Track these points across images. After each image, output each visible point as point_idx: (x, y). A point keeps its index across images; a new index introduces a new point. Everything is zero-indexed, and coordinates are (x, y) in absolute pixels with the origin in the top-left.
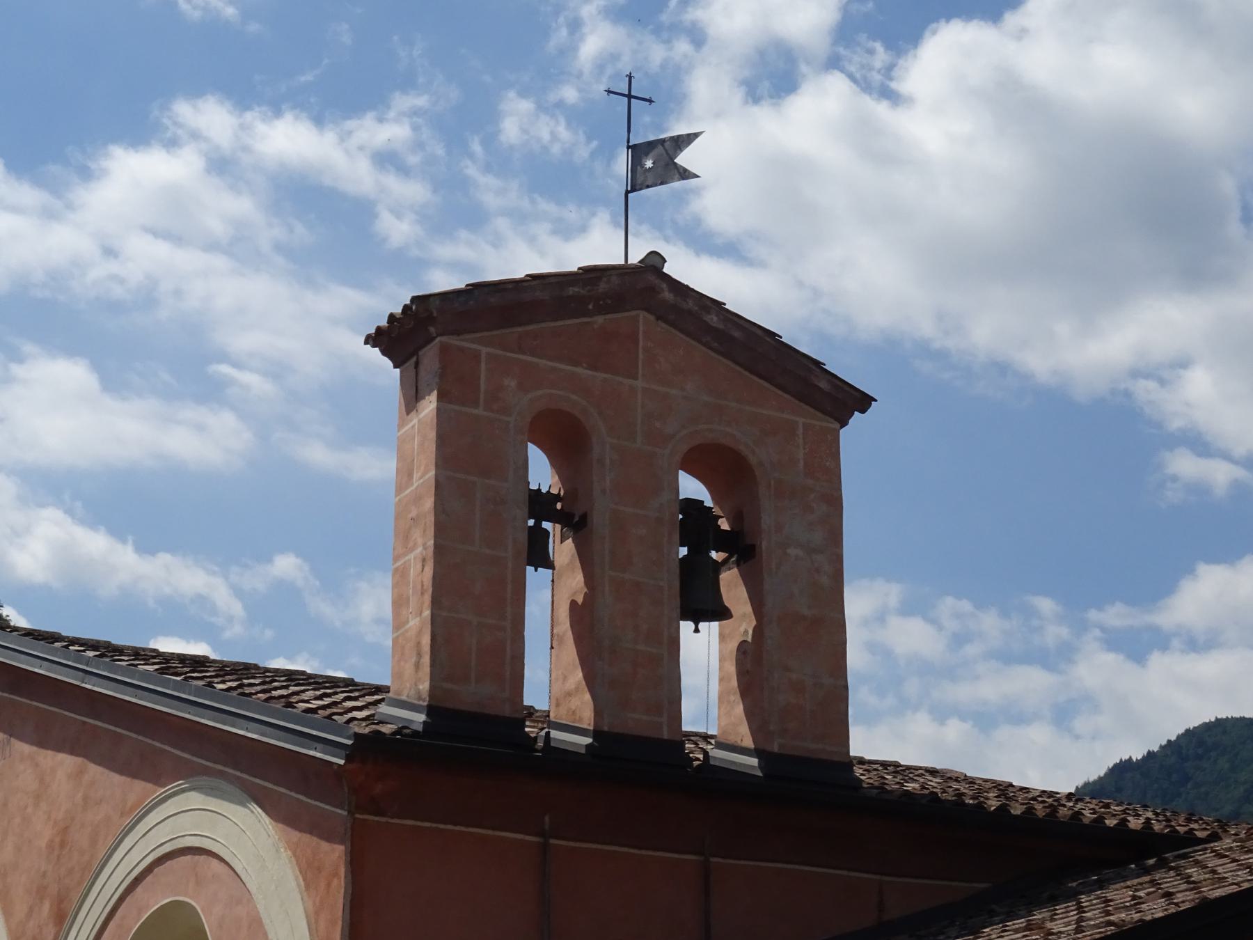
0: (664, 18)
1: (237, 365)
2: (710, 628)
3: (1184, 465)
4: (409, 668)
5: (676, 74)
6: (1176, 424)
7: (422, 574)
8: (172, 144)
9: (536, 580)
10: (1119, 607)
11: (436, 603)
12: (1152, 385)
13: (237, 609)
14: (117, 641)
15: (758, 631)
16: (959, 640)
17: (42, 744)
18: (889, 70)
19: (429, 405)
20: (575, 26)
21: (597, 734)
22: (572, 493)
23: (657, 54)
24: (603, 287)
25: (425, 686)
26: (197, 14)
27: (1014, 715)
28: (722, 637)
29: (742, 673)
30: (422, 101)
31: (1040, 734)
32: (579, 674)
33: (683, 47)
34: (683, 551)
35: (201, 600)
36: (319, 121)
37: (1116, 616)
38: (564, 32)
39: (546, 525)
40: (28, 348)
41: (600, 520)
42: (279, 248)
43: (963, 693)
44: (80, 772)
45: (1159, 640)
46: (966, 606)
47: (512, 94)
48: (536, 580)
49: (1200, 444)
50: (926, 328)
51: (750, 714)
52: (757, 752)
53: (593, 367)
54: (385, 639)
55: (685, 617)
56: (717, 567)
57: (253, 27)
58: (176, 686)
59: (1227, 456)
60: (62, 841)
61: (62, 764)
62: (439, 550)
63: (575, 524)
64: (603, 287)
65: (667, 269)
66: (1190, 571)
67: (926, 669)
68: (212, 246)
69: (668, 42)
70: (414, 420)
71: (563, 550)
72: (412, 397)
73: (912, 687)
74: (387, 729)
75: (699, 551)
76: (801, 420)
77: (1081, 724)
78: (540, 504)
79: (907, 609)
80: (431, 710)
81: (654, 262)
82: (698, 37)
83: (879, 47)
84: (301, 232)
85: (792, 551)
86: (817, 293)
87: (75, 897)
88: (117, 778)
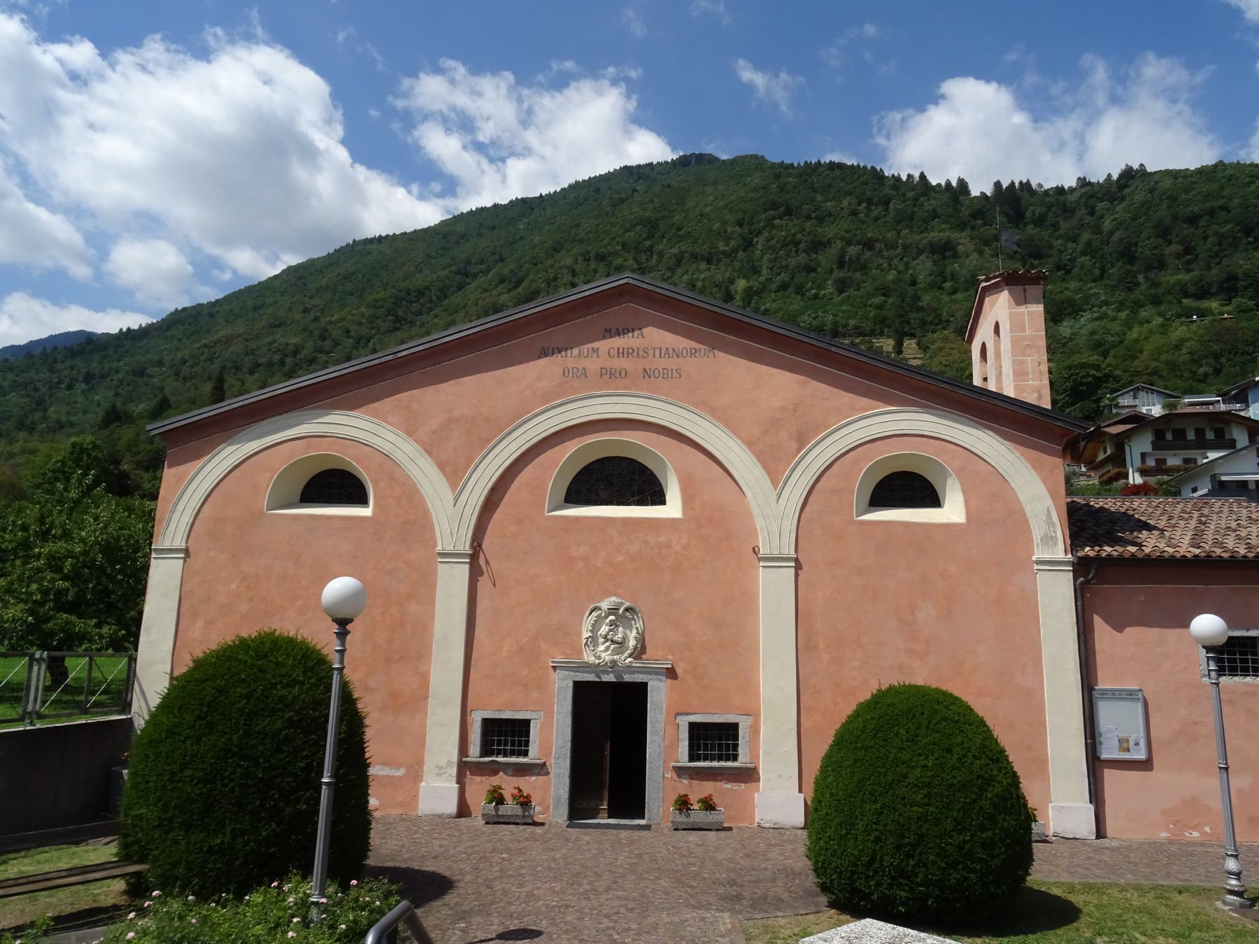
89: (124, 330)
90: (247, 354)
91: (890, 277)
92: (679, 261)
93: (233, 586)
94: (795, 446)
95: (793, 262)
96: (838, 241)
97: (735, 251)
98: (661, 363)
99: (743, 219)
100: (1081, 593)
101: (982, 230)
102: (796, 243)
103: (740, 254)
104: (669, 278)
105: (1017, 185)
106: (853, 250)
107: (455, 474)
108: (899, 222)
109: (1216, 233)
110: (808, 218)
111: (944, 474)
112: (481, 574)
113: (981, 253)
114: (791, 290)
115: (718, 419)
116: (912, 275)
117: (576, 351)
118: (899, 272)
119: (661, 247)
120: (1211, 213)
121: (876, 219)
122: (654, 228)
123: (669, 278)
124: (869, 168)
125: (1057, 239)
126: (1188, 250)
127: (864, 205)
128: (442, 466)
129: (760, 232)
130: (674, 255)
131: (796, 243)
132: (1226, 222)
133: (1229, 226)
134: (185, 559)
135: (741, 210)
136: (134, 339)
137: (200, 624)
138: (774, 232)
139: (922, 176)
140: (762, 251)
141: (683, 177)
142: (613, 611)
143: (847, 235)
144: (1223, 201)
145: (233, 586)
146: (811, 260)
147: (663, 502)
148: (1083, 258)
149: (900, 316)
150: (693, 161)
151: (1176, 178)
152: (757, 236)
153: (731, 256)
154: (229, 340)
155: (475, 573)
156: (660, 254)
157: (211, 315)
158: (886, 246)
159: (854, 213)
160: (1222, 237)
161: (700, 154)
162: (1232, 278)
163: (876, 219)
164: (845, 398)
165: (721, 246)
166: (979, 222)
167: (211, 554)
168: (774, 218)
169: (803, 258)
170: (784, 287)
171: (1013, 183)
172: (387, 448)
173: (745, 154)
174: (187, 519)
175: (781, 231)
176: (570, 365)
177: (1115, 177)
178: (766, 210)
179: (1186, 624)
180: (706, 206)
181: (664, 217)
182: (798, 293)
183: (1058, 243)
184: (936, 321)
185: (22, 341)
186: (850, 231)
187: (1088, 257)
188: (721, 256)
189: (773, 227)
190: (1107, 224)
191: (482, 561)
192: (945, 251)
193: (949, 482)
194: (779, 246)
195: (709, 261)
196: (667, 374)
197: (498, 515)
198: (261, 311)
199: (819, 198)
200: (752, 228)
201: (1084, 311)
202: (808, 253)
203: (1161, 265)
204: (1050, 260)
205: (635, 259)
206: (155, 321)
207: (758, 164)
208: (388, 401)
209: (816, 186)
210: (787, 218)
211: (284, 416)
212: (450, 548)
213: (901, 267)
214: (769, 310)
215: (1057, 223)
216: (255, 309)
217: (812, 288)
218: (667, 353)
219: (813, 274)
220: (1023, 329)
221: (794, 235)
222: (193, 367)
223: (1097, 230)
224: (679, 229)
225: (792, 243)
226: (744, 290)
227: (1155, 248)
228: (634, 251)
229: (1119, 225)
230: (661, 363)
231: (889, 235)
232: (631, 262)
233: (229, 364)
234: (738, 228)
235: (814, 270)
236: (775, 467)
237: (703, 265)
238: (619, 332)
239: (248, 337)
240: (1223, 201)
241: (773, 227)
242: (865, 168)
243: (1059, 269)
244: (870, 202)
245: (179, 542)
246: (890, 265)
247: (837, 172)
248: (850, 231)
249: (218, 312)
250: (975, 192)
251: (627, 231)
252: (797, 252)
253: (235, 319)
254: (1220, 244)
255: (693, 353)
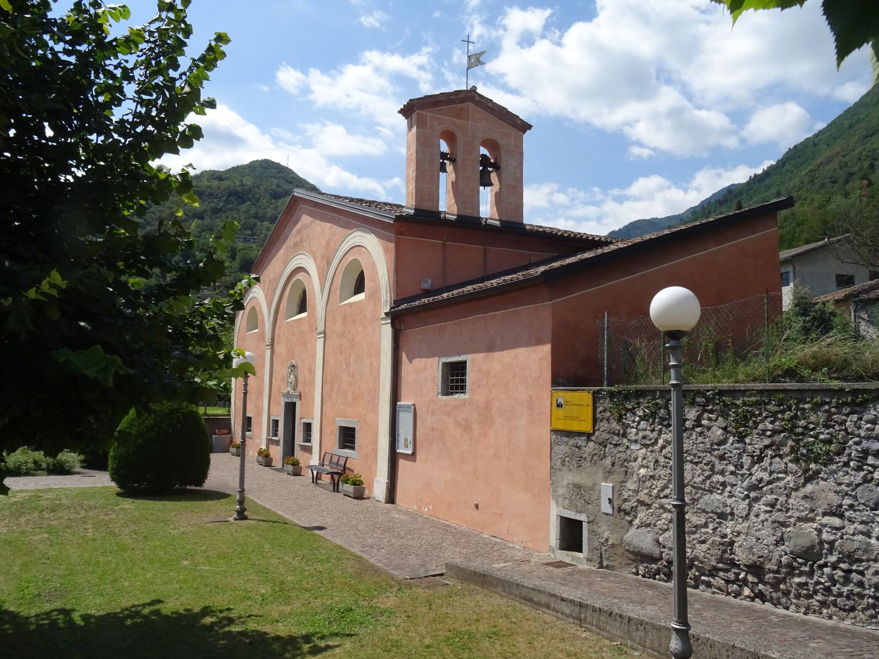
0: (497, 23)
1: (383, 127)
2: (488, 188)
3: (636, 150)
4: (410, 198)
5: (499, 39)
6: (634, 138)
7: (413, 175)
8: (365, 64)
9: (442, 175)
10: (617, 189)
11: (416, 182)
12: (628, 127)
13: (383, 192)
14: (341, 195)
15: (500, 189)
16: (573, 199)
17: (322, 220)
18: (561, 37)
19: (414, 129)
20: (472, 26)
21: (458, 215)
22: (452, 154)
23: (494, 33)
24: (460, 96)
25: (414, 203)
26: (368, 25)
27: (587, 219)
28: (491, 191)
29: (496, 200)
30: (430, 49)
31: (593, 224)
32: (454, 200)
33: (501, 32)
34: (481, 168)
35: (374, 190)
36: (403, 56)
37: (616, 192)
38: (469, 28)
39: (445, 161)
40: (328, 122)
41: (459, 160)
42: (393, 94)
43: (573, 213)
44: (332, 227)
45: (627, 198)
46: (575, 190)
47: (456, 48)
48: (442, 175)
49: (640, 144)
50: (568, 113)
51: (498, 210)
52: (500, 220)
53: (457, 119)
54: (404, 191)
55: (481, 185)
56: (490, 172)
57: (383, 29)
58: (353, 205)
59: (648, 148)
60: (328, 244)
61: (327, 225)
62: (417, 168)
63: (453, 161)
64: (460, 96)
65: (477, 91)
66: (637, 180)
67: (564, 207)
68: (375, 93)
69: (497, 30)
70: (411, 133)
71: (449, 167)
72: (410, 127)
73: (560, 212)
74: (404, 214)
75: (485, 168)
76: (513, 132)
77: (604, 221)
78: (444, 156)
79: (560, 191)
80: (415, 209)
81: (474, 89)
82: (505, 29)
83: (557, 31)
84: (398, 89)
85: (509, 168)
86: (537, 103)
87: (331, 258)
88: (340, 229)
89: (752, 176)
90: (841, 168)
136: (759, 181)
154: (829, 160)
157: (815, 145)
185: (696, 203)
198: (856, 128)
206: (774, 163)
216: (850, 127)
222: (799, 191)
233: (827, 181)
239: (846, 153)
249: (820, 140)
253: (835, 141)
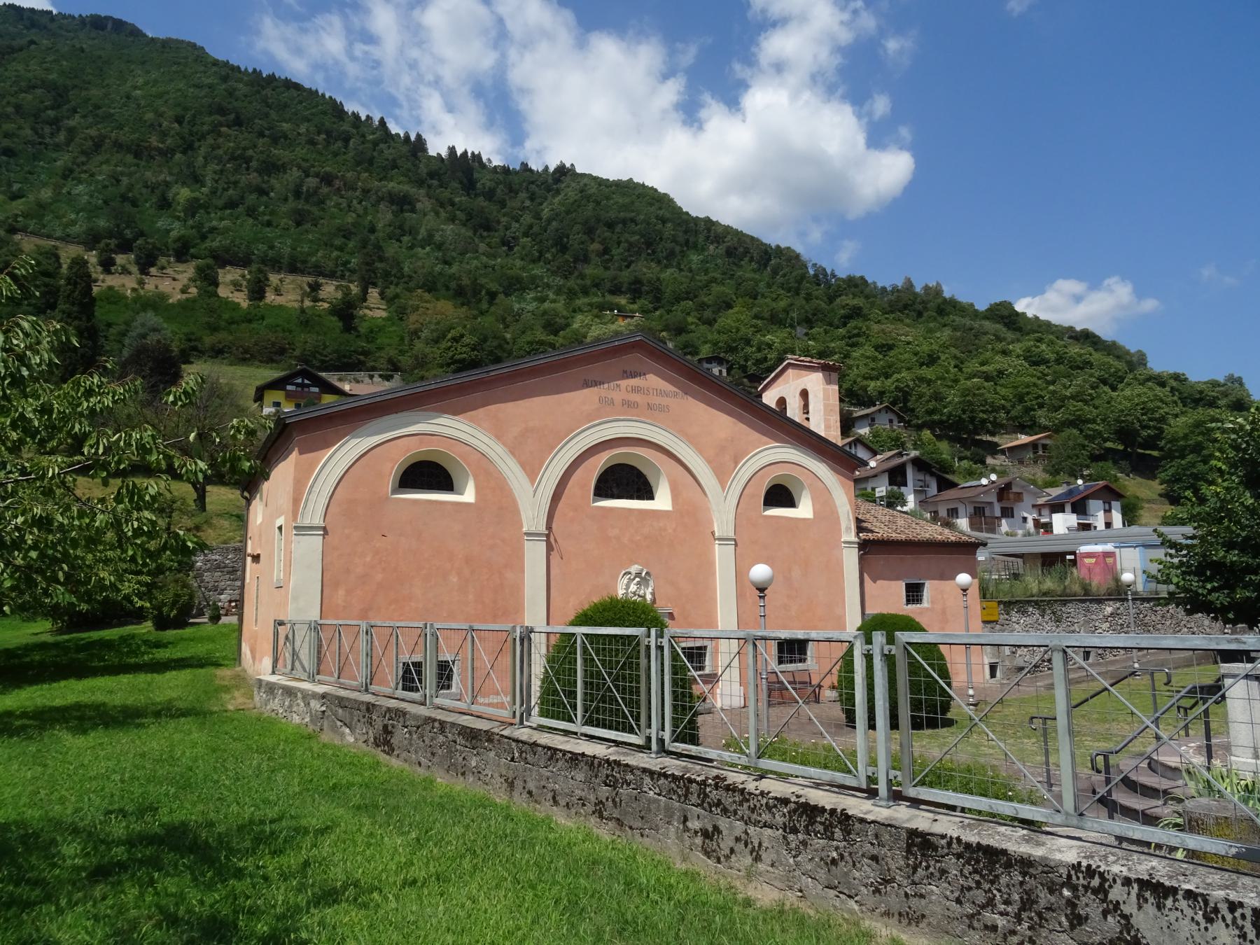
91: (350, 220)
92: (98, 145)
93: (368, 559)
94: (733, 465)
95: (244, 179)
96: (295, 169)
97: (172, 151)
98: (657, 400)
99: (183, 117)
100: (861, 559)
101: (438, 191)
102: (248, 160)
103: (178, 156)
104: (83, 164)
105: (469, 155)
106: (312, 182)
107: (532, 471)
108: (358, 163)
109: (627, 241)
110: (261, 135)
111: (802, 487)
112: (553, 550)
113: (437, 214)
114: (241, 209)
115: (691, 443)
116: (371, 222)
117: (606, 386)
118: (359, 216)
119: (72, 123)
120: (624, 222)
121: (336, 154)
122: (61, 96)
123: (83, 164)
124: (327, 96)
125: (504, 216)
126: (606, 251)
127: (324, 136)
128: (523, 465)
129: (203, 137)
130: (91, 137)
131: (248, 160)
132: (634, 233)
133: (637, 237)
134: (323, 535)
135: (179, 105)
137: (341, 592)
138: (221, 140)
139: (382, 122)
140: (205, 158)
141: (96, 41)
142: (638, 575)
143: (305, 165)
144: (633, 214)
145: (368, 559)
146: (264, 182)
147: (652, 498)
148: (525, 239)
149: (367, 264)
150: (109, 26)
151: (600, 185)
152: (199, 140)
153: (166, 155)
155: (550, 549)
156: (72, 131)
158: (345, 185)
159: (312, 142)
160: (631, 245)
161: (120, 21)
162: (638, 281)
163: (336, 154)
164: (756, 436)
165: (154, 141)
166: (435, 182)
167: (347, 531)
168: (222, 125)
169: (254, 178)
170: (232, 205)
171: (466, 152)
172: (483, 448)
173: (181, 37)
174: (323, 501)
175: (229, 141)
176: (603, 395)
177: (552, 169)
178: (210, 114)
179: (954, 578)
180: (136, 88)
181: (76, 86)
182: (250, 216)
183: (504, 220)
184: (399, 275)
186: (307, 161)
187: (529, 239)
188: (153, 153)
189: (220, 134)
190: (546, 213)
191: (552, 540)
192: (402, 203)
193: (804, 493)
194: (227, 157)
195: (137, 155)
196: (664, 409)
197: (561, 505)
199: (273, 115)
200: (195, 129)
201: (530, 290)
202: (260, 174)
203: (586, 260)
204: (496, 234)
205: (33, 129)
207: (198, 56)
208: (481, 410)
209: (270, 101)
210: (236, 128)
211: (400, 415)
212: (533, 530)
213: (361, 212)
214: (216, 229)
215: (504, 200)
217: (264, 214)
218: (665, 394)
219: (265, 198)
220: (829, 400)
221: (245, 149)
223: (538, 216)
224: (97, 107)
225: (241, 160)
226: (188, 200)
227: (583, 243)
228: (33, 118)
229: (555, 216)
230: (657, 400)
231: (349, 175)
232: (28, 132)
234: (176, 125)
235: (267, 194)
236: (723, 476)
237: (130, 158)
238: (633, 375)
240: (633, 214)
241: (220, 134)
242: (323, 95)
243: (504, 244)
244: (328, 133)
245: (318, 521)
246: (349, 207)
247: (294, 93)
248: (307, 161)
250: (432, 152)
251: (22, 91)
252: (248, 169)
254: (629, 251)
255: (676, 395)
